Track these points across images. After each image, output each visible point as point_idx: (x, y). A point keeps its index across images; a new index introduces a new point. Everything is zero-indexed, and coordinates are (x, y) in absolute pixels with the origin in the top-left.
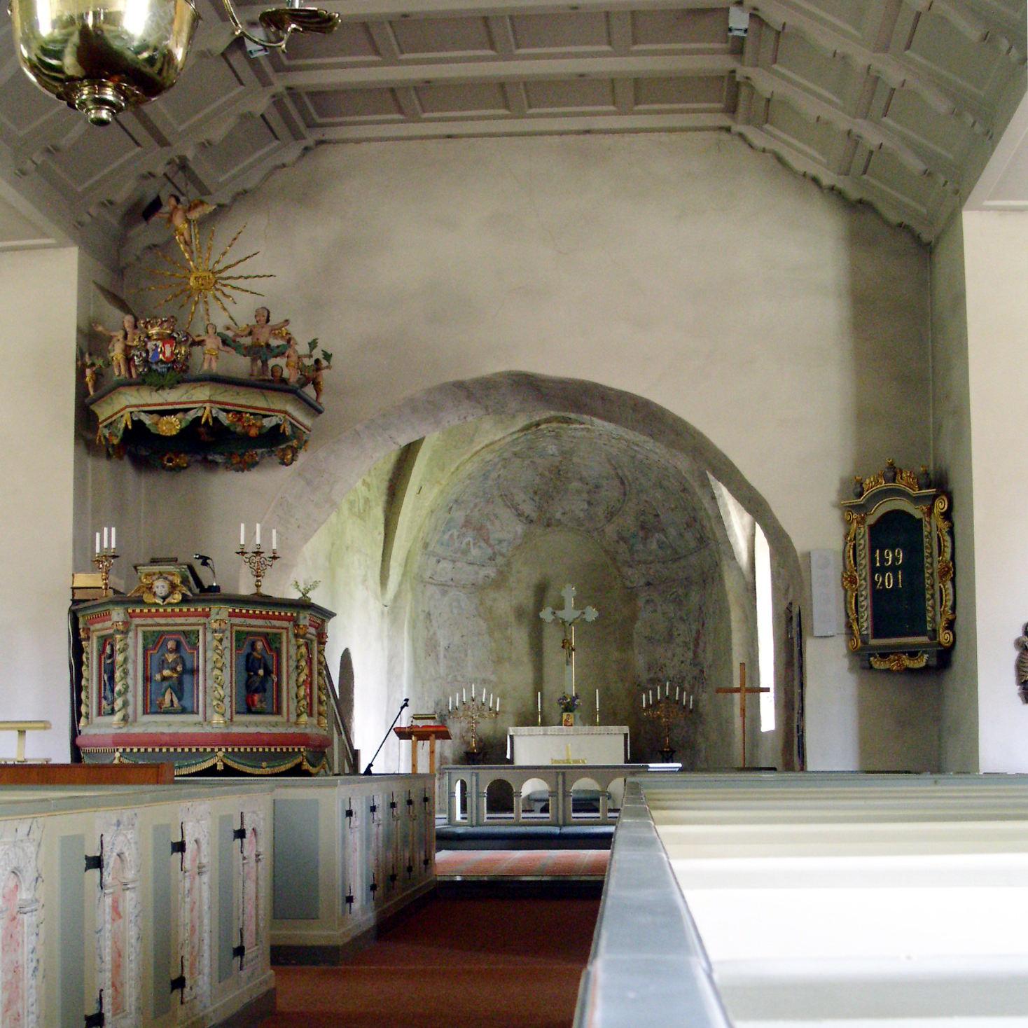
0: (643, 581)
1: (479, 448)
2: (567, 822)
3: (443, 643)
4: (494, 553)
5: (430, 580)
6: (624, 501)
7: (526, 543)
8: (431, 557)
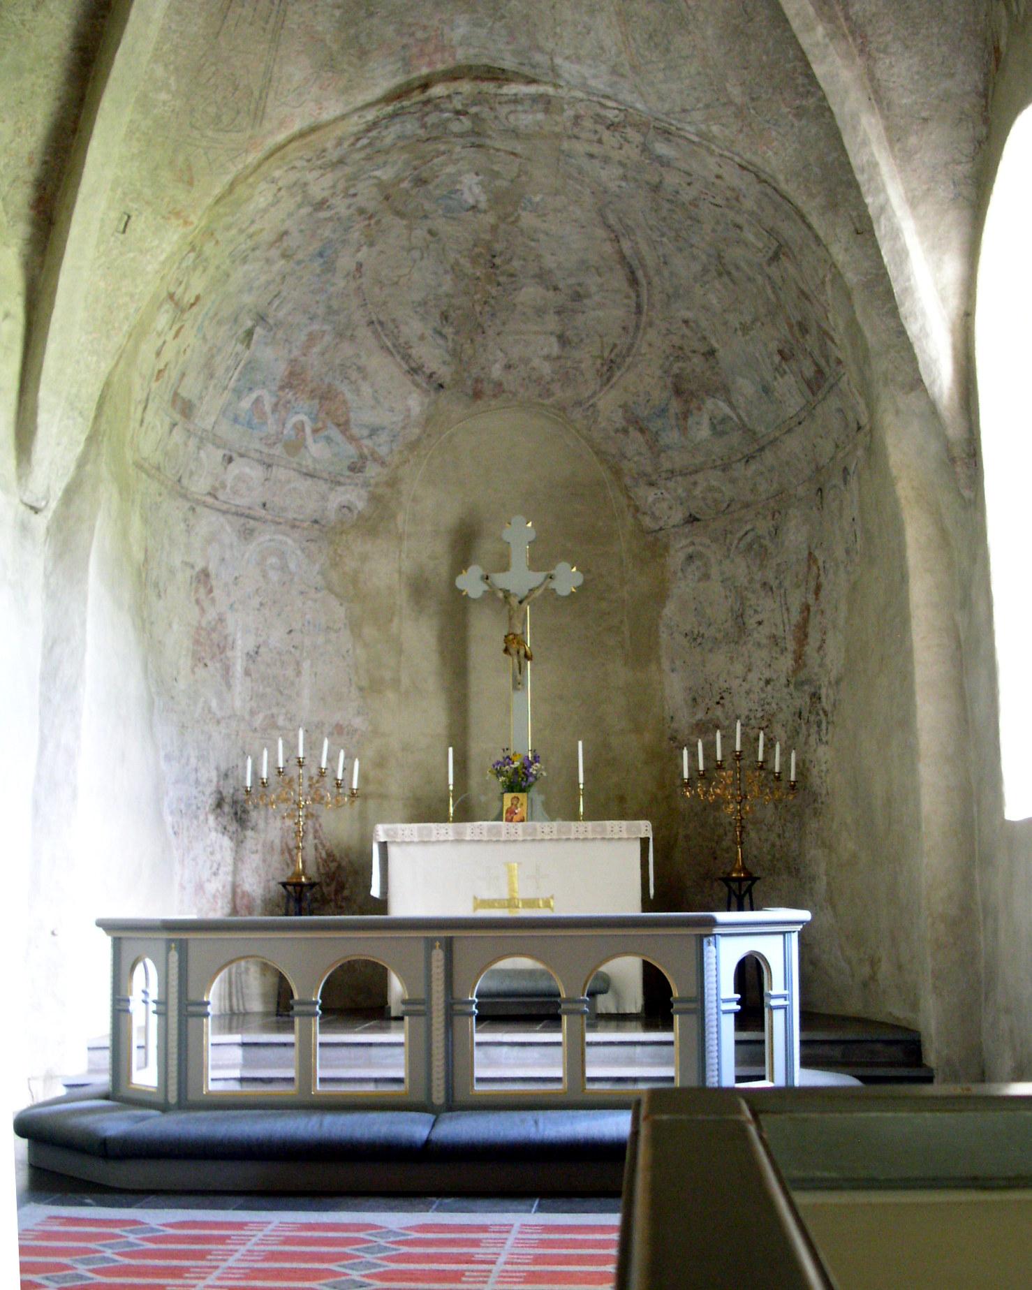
0: (678, 516)
1: (281, 137)
2: (460, 1097)
3: (242, 644)
4: (362, 457)
5: (210, 500)
6: (637, 327)
7: (429, 436)
8: (210, 447)
